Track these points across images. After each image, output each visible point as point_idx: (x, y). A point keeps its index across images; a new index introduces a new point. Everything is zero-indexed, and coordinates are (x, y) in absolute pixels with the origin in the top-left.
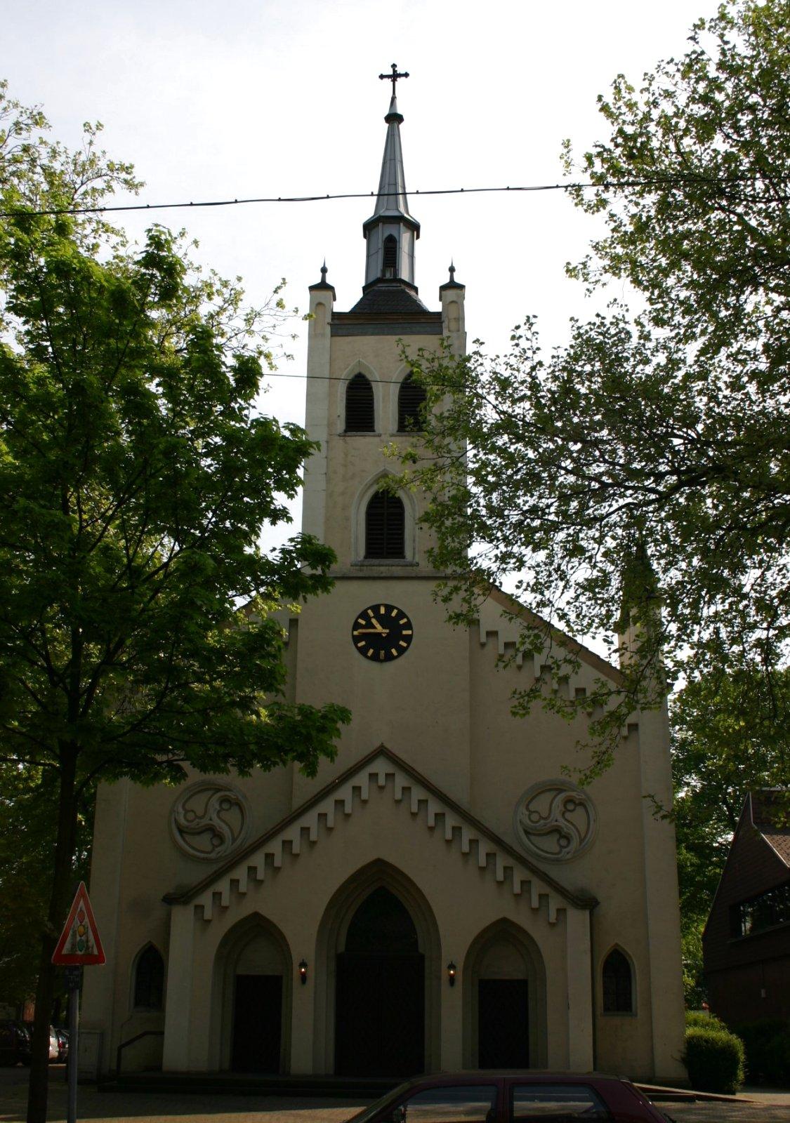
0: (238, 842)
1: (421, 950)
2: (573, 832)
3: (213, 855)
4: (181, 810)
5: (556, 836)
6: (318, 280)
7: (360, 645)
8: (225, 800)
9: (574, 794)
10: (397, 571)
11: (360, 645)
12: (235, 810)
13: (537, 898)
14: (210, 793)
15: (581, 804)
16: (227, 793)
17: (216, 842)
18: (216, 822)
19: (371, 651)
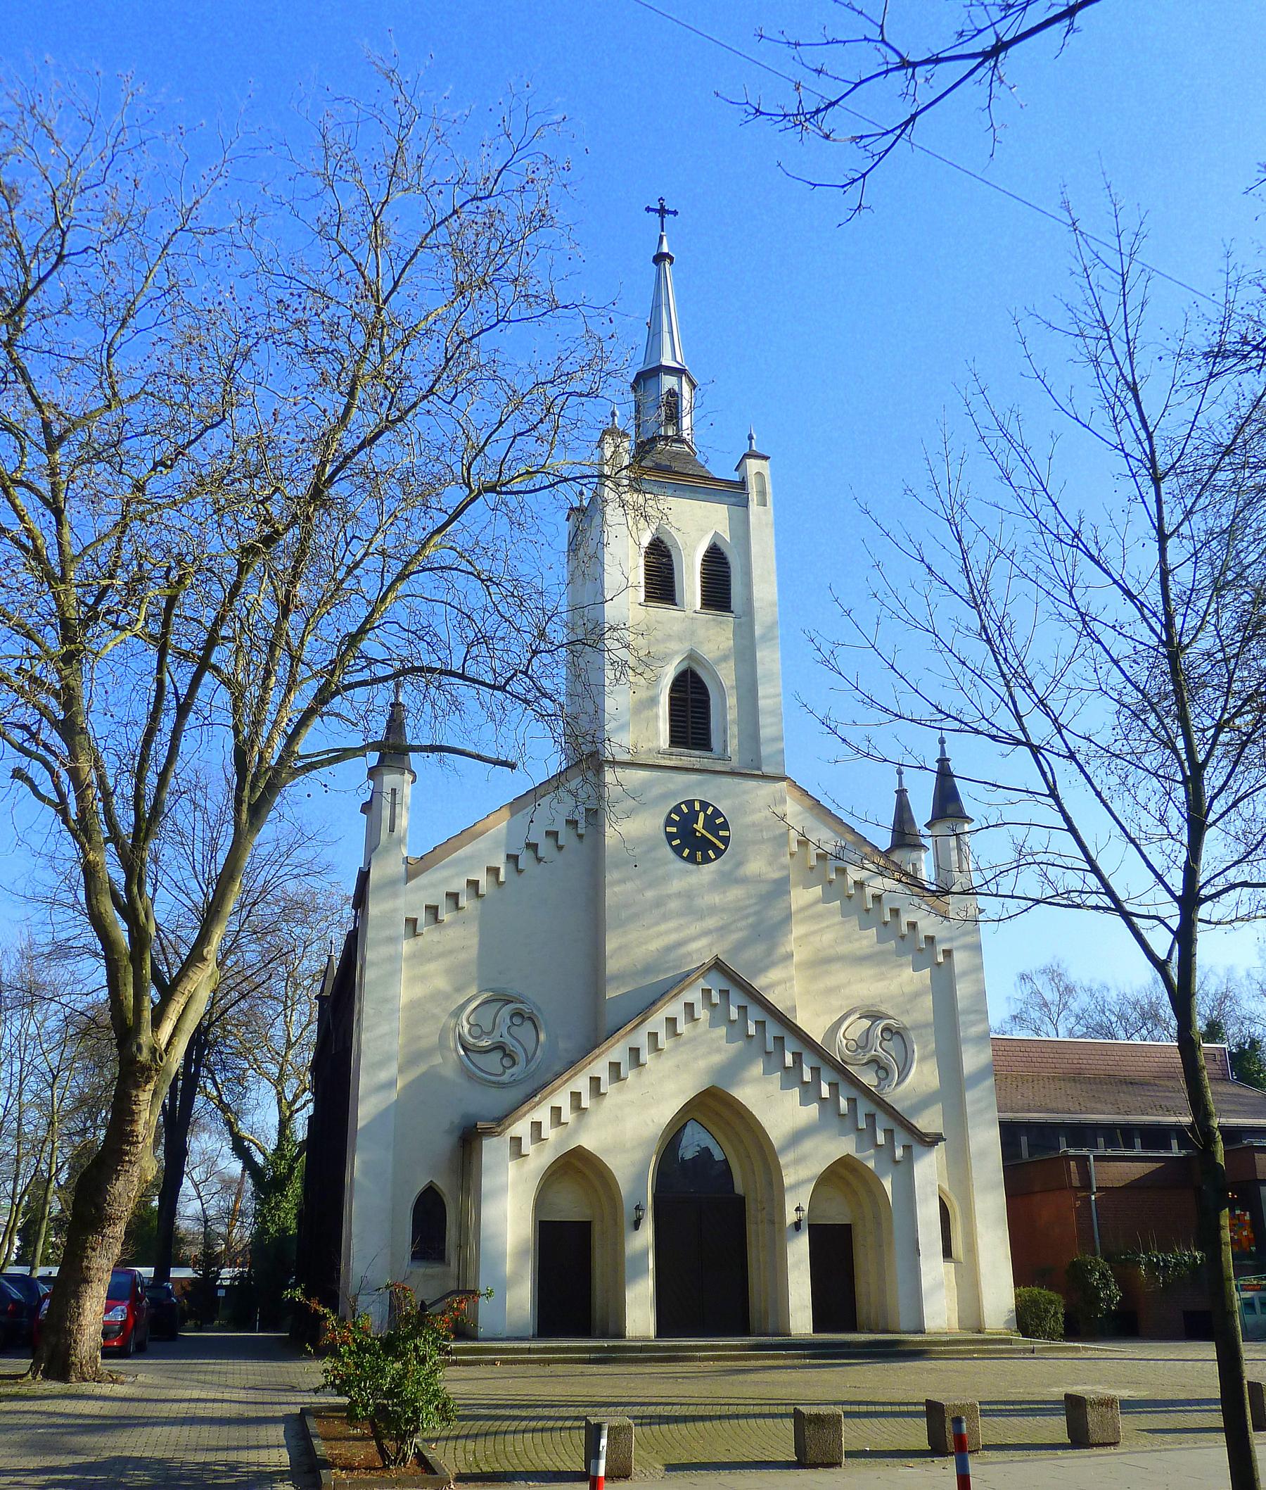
0: (533, 1065)
1: (739, 1188)
2: (520, 1050)
3: (505, 1078)
4: (465, 1023)
5: (500, 1055)
6: (747, 450)
7: (674, 843)
8: (518, 1014)
9: (891, 1021)
10: (706, 763)
11: (674, 843)
12: (528, 1024)
13: (994, 1134)
14: (500, 1004)
15: (897, 1033)
16: (891, 1021)
17: (507, 1062)
18: (507, 1039)
19: (687, 851)
